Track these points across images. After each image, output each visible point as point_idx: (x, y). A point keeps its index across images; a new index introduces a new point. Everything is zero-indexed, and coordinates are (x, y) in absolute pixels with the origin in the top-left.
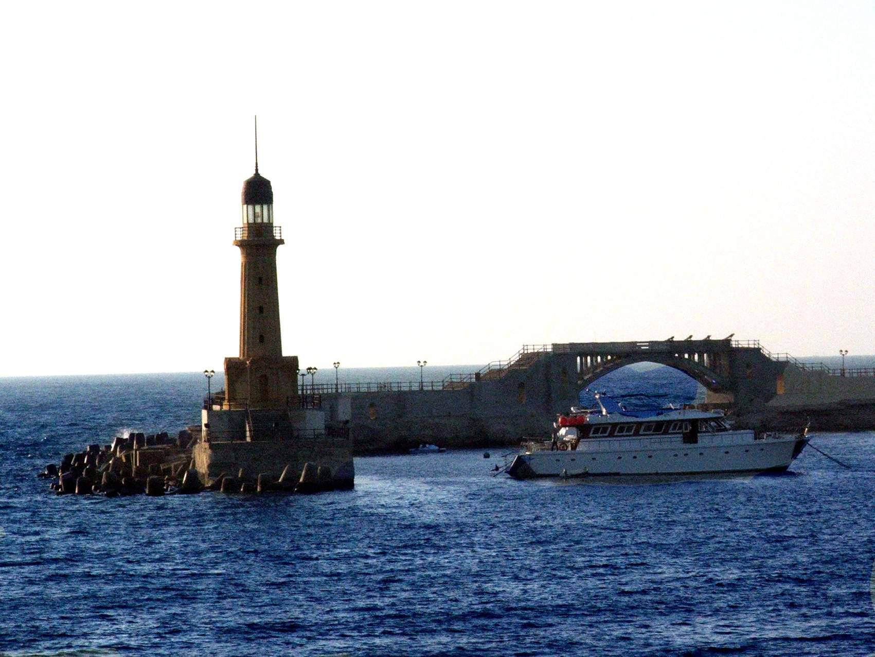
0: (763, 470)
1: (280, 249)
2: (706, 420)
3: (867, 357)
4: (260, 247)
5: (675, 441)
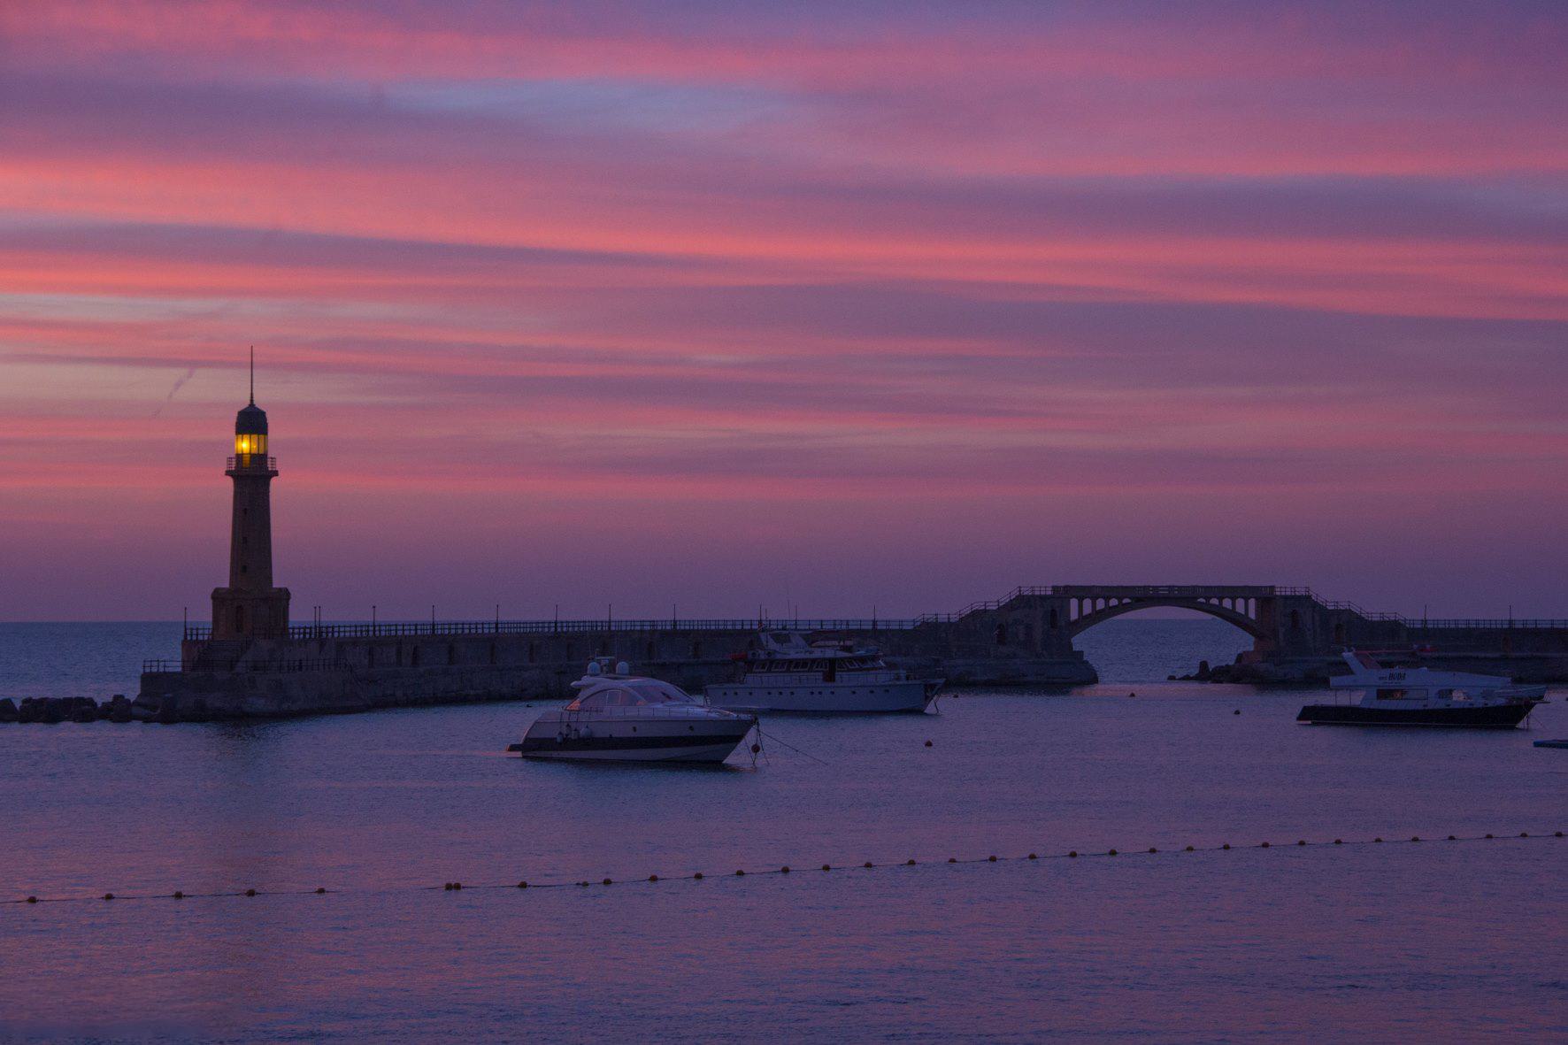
0: (930, 634)
1: (274, 482)
4: (252, 479)
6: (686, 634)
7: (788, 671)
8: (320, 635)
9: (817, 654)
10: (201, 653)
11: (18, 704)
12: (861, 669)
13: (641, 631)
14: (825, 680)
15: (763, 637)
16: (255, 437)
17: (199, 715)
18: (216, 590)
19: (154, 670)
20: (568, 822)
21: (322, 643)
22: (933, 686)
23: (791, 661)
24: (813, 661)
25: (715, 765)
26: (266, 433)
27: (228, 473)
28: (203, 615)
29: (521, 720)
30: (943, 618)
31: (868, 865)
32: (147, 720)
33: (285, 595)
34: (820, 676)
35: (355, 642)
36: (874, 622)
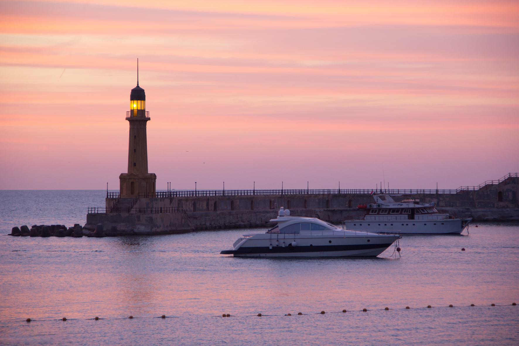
0: (464, 195)
1: (148, 123)
2: (418, 208)
3: (102, 191)
4: (138, 122)
5: (404, 217)
6: (345, 196)
7: (389, 214)
8: (170, 196)
9: (405, 206)
10: (115, 204)
11: (30, 228)
12: (428, 213)
13: (323, 194)
14: (409, 218)
15: (375, 197)
16: (139, 102)
17: (113, 233)
18: (122, 174)
19: (93, 212)
20: (260, 285)
22: (466, 222)
23: (390, 209)
24: (402, 209)
25: (374, 257)
26: (144, 100)
27: (127, 119)
28: (115, 187)
29: (231, 239)
30: (471, 189)
31: (365, 310)
32: (89, 236)
33: (153, 177)
34: (407, 216)
35: (187, 199)
36: (437, 191)
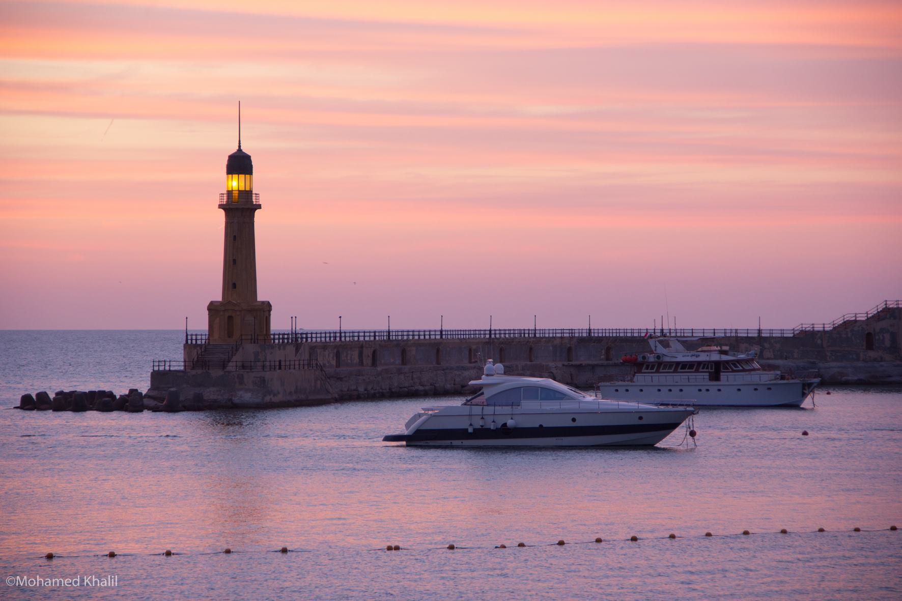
0: (806, 339)
1: (258, 213)
2: (727, 362)
4: (240, 212)
5: (702, 377)
6: (599, 340)
7: (675, 371)
8: (296, 340)
9: (703, 357)
10: (200, 354)
11: (52, 396)
12: (744, 370)
13: (562, 338)
14: (711, 379)
15: (652, 342)
16: (242, 176)
17: (196, 405)
18: (212, 303)
19: (162, 368)
20: (451, 496)
21: (298, 346)
22: (810, 385)
23: (678, 363)
24: (699, 363)
25: (649, 447)
26: (251, 173)
27: (221, 206)
28: (200, 324)
29: (401, 415)
30: (818, 328)
31: (634, 539)
32: (155, 409)
34: (706, 376)
35: (325, 346)
36: (760, 331)
